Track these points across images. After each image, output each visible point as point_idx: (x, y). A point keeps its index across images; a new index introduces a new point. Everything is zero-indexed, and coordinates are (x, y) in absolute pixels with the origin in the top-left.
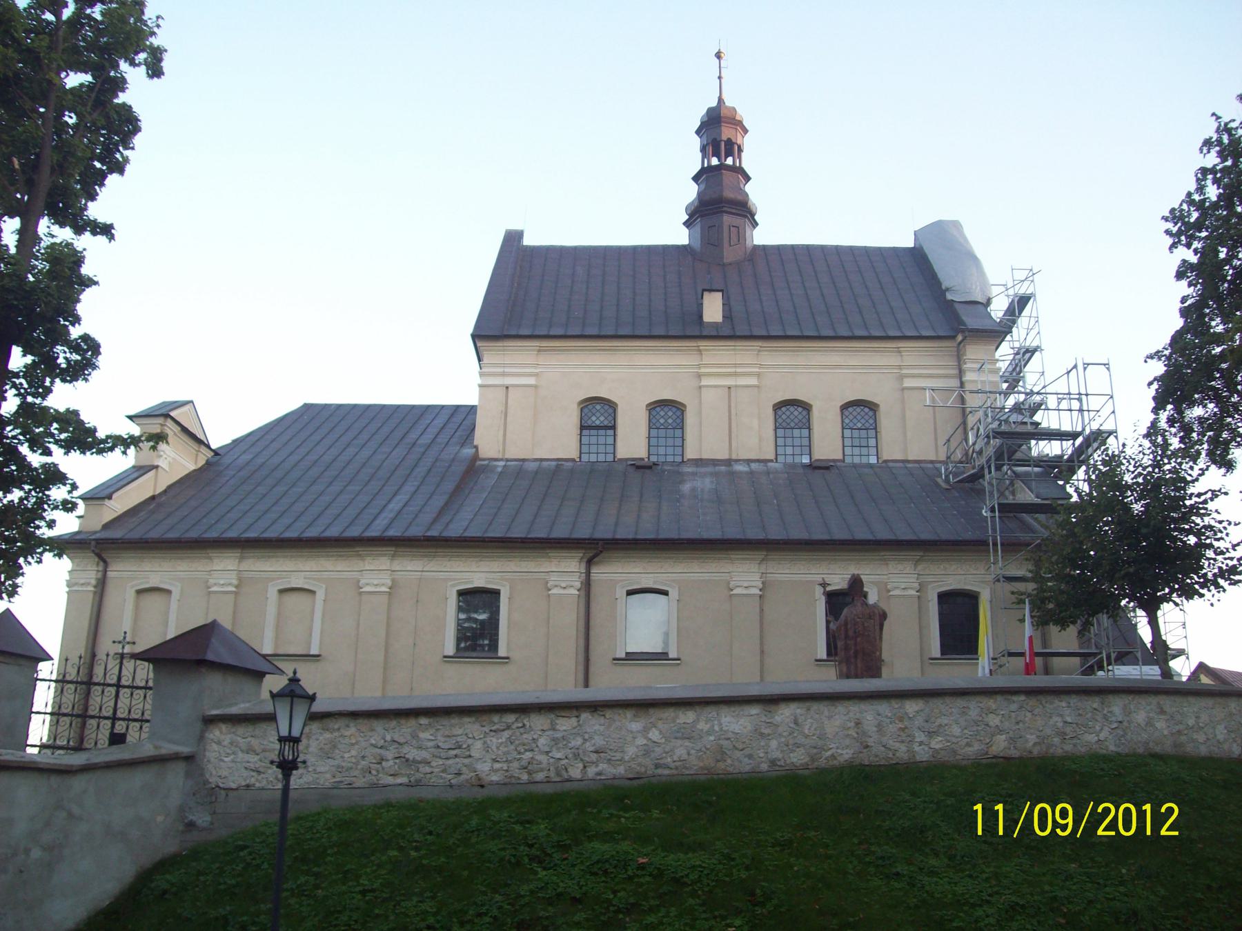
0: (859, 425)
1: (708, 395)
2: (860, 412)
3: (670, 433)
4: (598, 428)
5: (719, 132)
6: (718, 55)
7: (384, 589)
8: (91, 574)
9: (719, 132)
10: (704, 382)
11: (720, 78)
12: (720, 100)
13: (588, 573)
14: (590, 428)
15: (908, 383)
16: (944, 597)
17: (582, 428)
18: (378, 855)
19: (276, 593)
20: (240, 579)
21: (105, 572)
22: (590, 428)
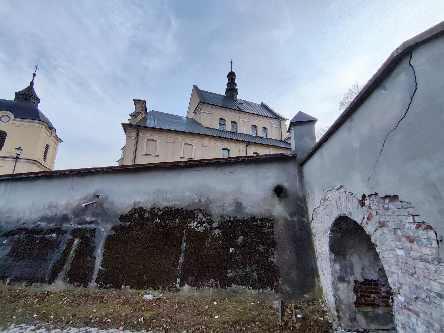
5: (232, 76)
6: (231, 62)
9: (232, 76)
15: (272, 125)
21: (138, 134)
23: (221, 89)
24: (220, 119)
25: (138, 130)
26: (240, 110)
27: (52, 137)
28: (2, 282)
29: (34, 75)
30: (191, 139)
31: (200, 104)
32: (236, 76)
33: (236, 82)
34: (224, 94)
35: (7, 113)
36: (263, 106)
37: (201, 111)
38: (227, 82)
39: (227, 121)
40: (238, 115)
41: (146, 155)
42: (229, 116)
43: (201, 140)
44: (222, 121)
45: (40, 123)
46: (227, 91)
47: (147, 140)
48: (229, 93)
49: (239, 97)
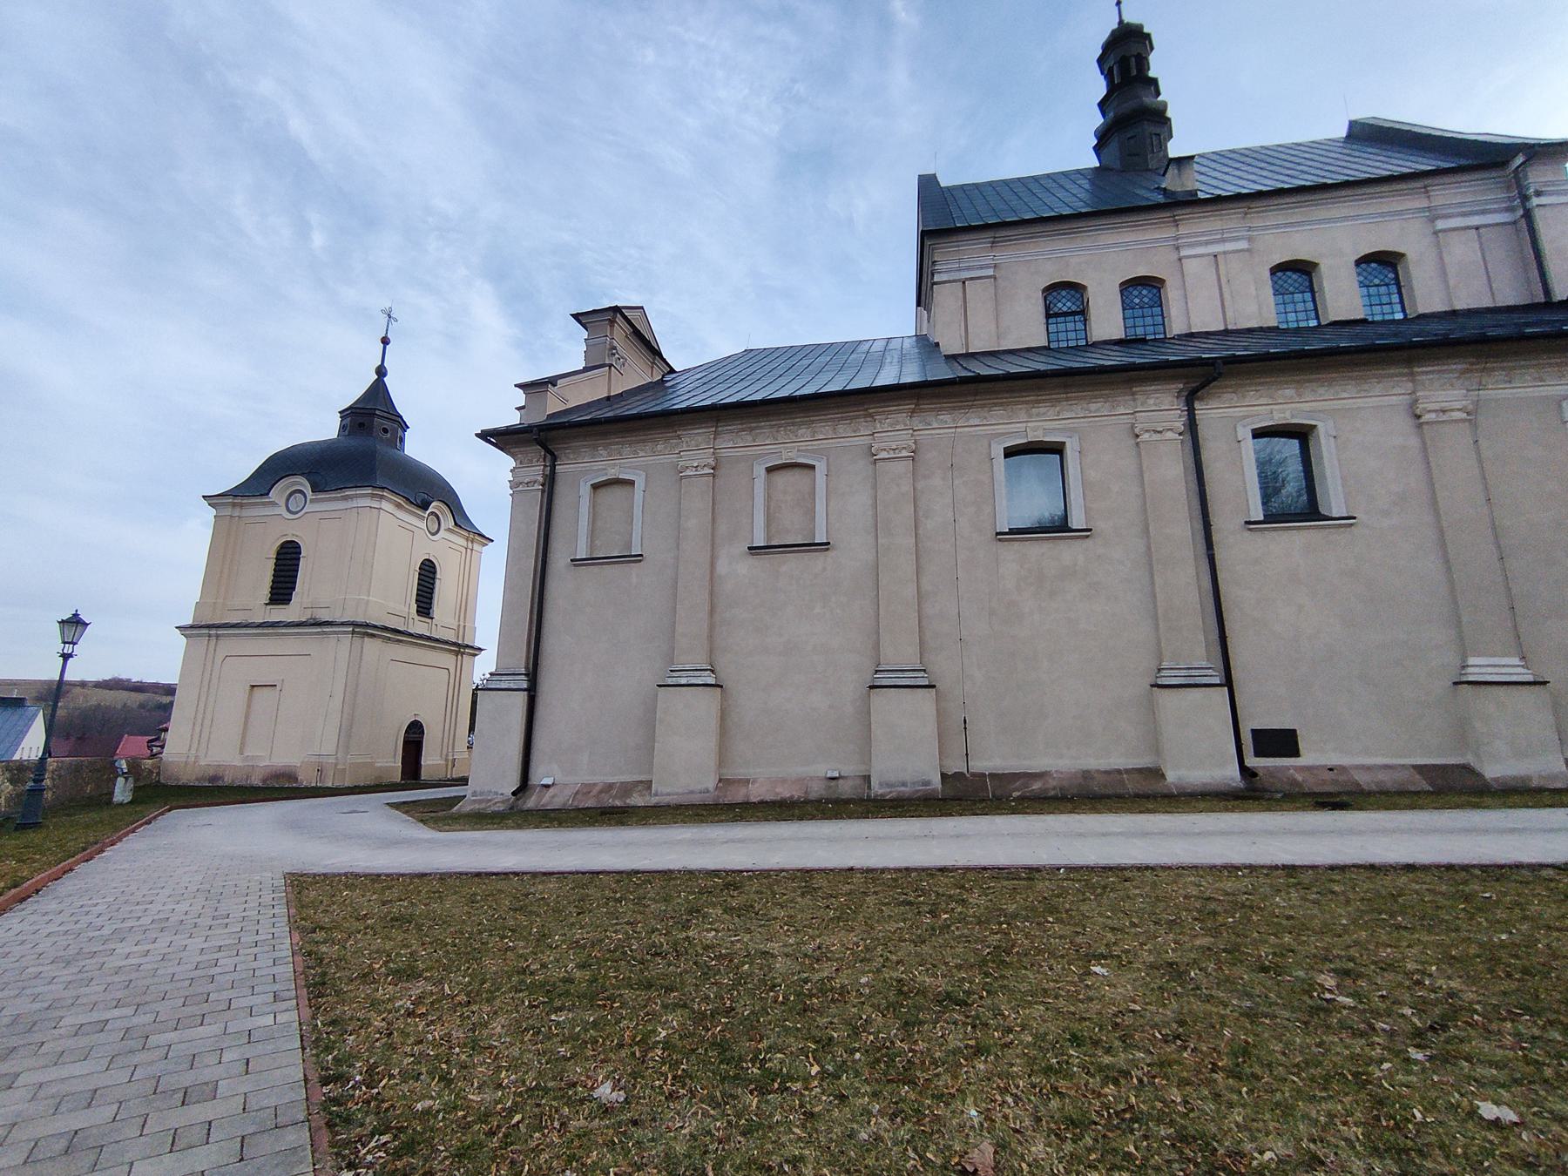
0: (1377, 281)
1: (1191, 266)
2: (1382, 265)
3: (1147, 311)
4: (1065, 314)
5: (1126, 55)
7: (904, 453)
8: (536, 472)
9: (1126, 55)
10: (1183, 253)
12: (1121, 22)
14: (1057, 315)
15: (1440, 225)
17: (1048, 316)
18: (1518, 939)
19: (763, 472)
21: (553, 467)
22: (1057, 315)
23: (1060, 137)
24: (1051, 290)
25: (548, 451)
26: (1190, 202)
27: (442, 533)
28: (874, 782)
29: (385, 341)
31: (927, 243)
32: (1148, 36)
34: (1094, 162)
35: (294, 484)
36: (1366, 135)
37: (936, 279)
38: (1100, 88)
40: (1169, 232)
41: (591, 561)
42: (1103, 262)
44: (1064, 299)
45: (373, 496)
46: (1103, 138)
47: (770, 470)
48: (1113, 147)
49: (1175, 149)
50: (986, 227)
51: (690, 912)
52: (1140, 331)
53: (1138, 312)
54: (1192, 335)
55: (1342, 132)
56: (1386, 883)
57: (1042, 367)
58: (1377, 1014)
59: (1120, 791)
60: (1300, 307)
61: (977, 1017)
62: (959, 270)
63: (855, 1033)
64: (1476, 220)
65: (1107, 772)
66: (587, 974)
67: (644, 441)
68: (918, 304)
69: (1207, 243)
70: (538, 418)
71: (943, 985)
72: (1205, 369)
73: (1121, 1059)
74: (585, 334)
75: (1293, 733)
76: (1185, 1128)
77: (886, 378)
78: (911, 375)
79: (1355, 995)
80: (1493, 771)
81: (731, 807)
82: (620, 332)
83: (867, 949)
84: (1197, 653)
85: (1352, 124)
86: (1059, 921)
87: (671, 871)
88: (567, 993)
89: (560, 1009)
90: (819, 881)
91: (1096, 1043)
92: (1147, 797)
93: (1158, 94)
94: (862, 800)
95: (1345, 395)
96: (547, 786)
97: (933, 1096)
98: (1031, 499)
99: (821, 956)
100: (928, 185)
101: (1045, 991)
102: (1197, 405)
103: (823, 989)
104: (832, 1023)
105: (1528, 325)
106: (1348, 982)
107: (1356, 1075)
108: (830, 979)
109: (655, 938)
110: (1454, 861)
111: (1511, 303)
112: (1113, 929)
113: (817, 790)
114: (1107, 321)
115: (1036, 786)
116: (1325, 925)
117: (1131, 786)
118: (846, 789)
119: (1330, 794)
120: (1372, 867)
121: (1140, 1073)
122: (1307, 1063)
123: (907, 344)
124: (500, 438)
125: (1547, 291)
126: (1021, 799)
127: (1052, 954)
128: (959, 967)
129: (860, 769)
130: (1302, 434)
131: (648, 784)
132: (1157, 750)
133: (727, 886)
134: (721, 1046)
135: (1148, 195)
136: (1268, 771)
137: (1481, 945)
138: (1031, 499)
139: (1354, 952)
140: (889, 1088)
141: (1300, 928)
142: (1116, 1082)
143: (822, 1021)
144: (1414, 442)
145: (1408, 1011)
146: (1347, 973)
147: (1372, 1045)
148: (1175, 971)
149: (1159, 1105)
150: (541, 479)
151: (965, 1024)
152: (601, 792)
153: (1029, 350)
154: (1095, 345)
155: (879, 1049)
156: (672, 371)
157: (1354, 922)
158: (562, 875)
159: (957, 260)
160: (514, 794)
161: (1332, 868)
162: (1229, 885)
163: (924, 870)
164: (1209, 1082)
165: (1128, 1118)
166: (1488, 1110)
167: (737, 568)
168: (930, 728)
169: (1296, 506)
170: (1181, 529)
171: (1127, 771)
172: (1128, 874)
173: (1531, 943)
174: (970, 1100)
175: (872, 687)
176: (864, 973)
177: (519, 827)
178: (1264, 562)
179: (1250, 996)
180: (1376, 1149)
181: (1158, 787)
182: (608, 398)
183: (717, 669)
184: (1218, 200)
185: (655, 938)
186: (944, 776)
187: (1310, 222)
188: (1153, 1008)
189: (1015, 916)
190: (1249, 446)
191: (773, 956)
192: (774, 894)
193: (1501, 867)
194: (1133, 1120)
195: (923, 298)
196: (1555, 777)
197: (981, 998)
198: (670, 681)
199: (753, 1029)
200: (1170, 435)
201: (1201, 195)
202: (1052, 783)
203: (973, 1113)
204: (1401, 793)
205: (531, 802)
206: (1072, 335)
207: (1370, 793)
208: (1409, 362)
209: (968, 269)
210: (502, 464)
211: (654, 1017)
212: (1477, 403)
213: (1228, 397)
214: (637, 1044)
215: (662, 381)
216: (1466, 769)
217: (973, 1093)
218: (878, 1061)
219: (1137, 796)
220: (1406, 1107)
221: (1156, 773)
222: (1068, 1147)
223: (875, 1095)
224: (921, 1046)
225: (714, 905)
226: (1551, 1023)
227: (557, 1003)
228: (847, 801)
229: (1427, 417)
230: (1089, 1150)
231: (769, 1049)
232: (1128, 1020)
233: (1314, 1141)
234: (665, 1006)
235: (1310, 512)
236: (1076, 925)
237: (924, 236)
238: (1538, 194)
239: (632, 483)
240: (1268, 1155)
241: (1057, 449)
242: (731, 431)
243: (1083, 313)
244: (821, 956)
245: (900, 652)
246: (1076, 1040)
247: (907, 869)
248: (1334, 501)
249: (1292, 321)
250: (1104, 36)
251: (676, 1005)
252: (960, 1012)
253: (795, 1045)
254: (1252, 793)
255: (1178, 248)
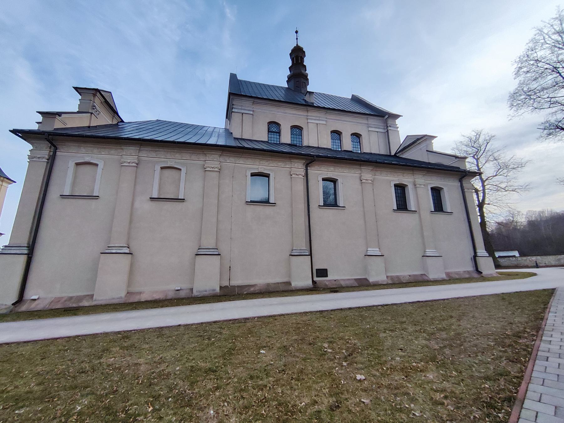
2: (356, 136)
5: (298, 55)
6: (297, 32)
7: (216, 170)
8: (45, 153)
9: (298, 55)
11: (297, 39)
12: (297, 45)
13: (307, 170)
14: (271, 132)
15: (370, 129)
16: (432, 189)
17: (269, 131)
19: (159, 168)
20: (139, 160)
22: (271, 132)
23: (278, 76)
24: (270, 123)
25: (52, 144)
26: (309, 106)
28: (194, 291)
30: (178, 156)
31: (231, 97)
32: (304, 52)
33: (304, 64)
36: (356, 100)
37: (233, 110)
39: (282, 127)
40: (305, 114)
42: (287, 118)
43: (202, 158)
44: (274, 127)
46: (290, 79)
48: (292, 82)
49: (309, 89)
50: (251, 97)
51: (103, 351)
52: (295, 142)
53: (295, 136)
54: (309, 147)
55: (350, 98)
56: (344, 313)
57: (265, 148)
58: (337, 353)
59: (278, 290)
60: (337, 144)
61: (219, 375)
62: (241, 109)
63: (171, 390)
64: (377, 130)
65: (275, 284)
66: (42, 387)
67: (105, 148)
68: (227, 118)
69: (315, 120)
70: (48, 128)
71: (208, 365)
72: (312, 158)
73: (264, 382)
74: (80, 97)
75: (326, 270)
76: (280, 400)
77: (212, 141)
78: (221, 142)
79: (332, 349)
80: (372, 280)
81: (132, 304)
82: (97, 101)
83: (181, 356)
84: (303, 246)
85: (353, 95)
86: (253, 336)
87: (97, 334)
88: (28, 399)
89: (22, 407)
90: (167, 332)
91: (258, 377)
92: (286, 291)
93: (306, 70)
94: (188, 298)
95: (103, 153)
96: (35, 300)
97: (198, 409)
98: (257, 191)
99: (162, 361)
100: (233, 77)
101: (244, 362)
102: (309, 168)
103: (160, 375)
104: (161, 389)
105: (386, 160)
106: (331, 345)
107: (329, 373)
108: (163, 370)
109: (83, 365)
110: (360, 306)
111: (383, 154)
112: (269, 337)
113: (171, 295)
114: (286, 137)
115: (252, 289)
116: (328, 328)
117: (282, 288)
118: (183, 294)
119: (334, 288)
120: (341, 309)
121: (270, 385)
122: (317, 372)
123: (221, 131)
124: (25, 135)
125: (390, 152)
126: (247, 294)
127: (249, 349)
128: (215, 358)
129: (189, 286)
130: (334, 181)
131: (92, 296)
132: (290, 276)
133: (123, 338)
134: (107, 408)
135: (299, 99)
136: (321, 281)
137: (363, 329)
138: (257, 191)
139: (334, 336)
140: (181, 410)
141: (321, 330)
142: (262, 390)
143: (157, 388)
144: (360, 187)
145: (344, 351)
146: (331, 342)
147: (334, 363)
148: (285, 348)
149: (274, 395)
150: (47, 157)
151: (214, 379)
152: (65, 301)
153: (262, 141)
154: (282, 144)
155: (180, 395)
156: (122, 121)
157: (335, 326)
158: (35, 342)
159: (241, 105)
160: (13, 304)
161: (332, 310)
162: (305, 318)
163: (208, 323)
164: (290, 384)
165: (263, 402)
166: (359, 377)
167: (144, 206)
168: (217, 270)
169: (331, 202)
170: (302, 206)
171: (281, 283)
172: (276, 318)
173: (373, 328)
174: (211, 408)
175: (196, 255)
176: (178, 366)
177: (14, 320)
178: (323, 217)
179: (305, 353)
180: (331, 395)
181: (290, 288)
182: (89, 127)
183: (130, 246)
184: (318, 107)
185: (83, 365)
186: (221, 287)
187: (341, 120)
188: (277, 362)
189: (238, 336)
190: (321, 183)
191: (140, 365)
192: (145, 339)
193: (370, 306)
194: (265, 402)
195: (228, 116)
196: (384, 281)
197: (222, 368)
198: (107, 251)
199: (125, 398)
200: (300, 176)
201: (315, 105)
202: (257, 288)
203: (212, 412)
204: (352, 287)
205: (24, 308)
206: (275, 140)
207: (344, 287)
208: (360, 165)
209: (245, 110)
210: (25, 148)
211: (75, 401)
212: (374, 179)
213: (316, 167)
214: (64, 416)
215: (117, 124)
216: (366, 279)
217: (213, 405)
218: (178, 400)
219: (283, 291)
220: (340, 380)
221: (289, 283)
222: (243, 417)
223: (175, 414)
224: (197, 390)
225: (116, 347)
226: (375, 349)
227: (21, 404)
228: (183, 299)
229: (364, 181)
230: (250, 416)
231: (131, 405)
232: (269, 367)
233: (315, 396)
234: (82, 396)
235: (335, 204)
236: (257, 337)
237: (230, 94)
238: (390, 126)
239: (97, 165)
240: (303, 403)
241: (267, 176)
242: (147, 150)
243: (279, 133)
244: (162, 361)
245: (209, 242)
246: (252, 378)
247: (202, 323)
248: (341, 203)
249: (335, 148)
250: (292, 47)
251: (87, 394)
252: (213, 375)
253: (143, 400)
254: (315, 289)
255: (307, 119)
